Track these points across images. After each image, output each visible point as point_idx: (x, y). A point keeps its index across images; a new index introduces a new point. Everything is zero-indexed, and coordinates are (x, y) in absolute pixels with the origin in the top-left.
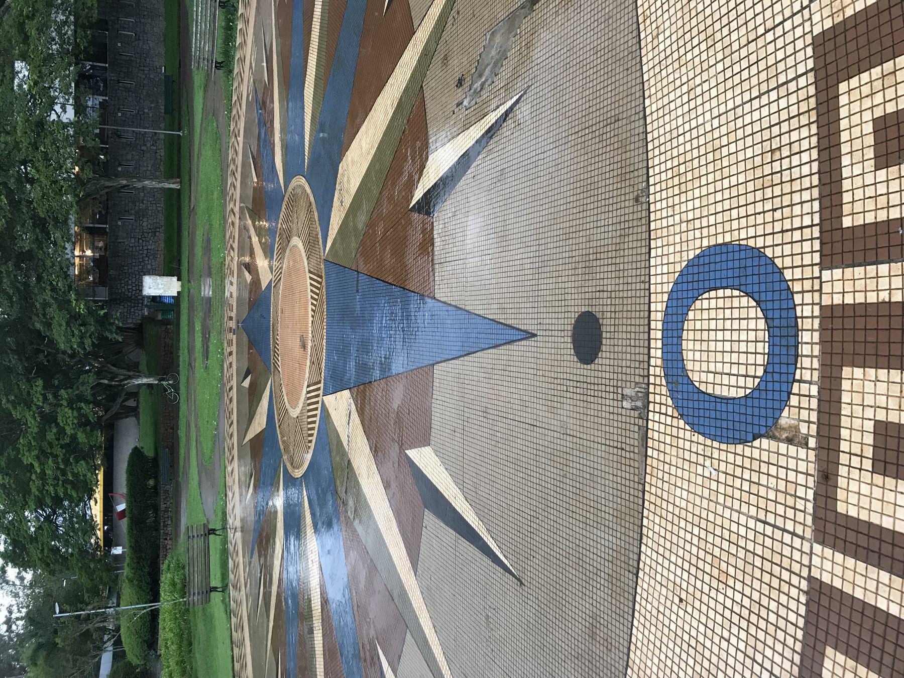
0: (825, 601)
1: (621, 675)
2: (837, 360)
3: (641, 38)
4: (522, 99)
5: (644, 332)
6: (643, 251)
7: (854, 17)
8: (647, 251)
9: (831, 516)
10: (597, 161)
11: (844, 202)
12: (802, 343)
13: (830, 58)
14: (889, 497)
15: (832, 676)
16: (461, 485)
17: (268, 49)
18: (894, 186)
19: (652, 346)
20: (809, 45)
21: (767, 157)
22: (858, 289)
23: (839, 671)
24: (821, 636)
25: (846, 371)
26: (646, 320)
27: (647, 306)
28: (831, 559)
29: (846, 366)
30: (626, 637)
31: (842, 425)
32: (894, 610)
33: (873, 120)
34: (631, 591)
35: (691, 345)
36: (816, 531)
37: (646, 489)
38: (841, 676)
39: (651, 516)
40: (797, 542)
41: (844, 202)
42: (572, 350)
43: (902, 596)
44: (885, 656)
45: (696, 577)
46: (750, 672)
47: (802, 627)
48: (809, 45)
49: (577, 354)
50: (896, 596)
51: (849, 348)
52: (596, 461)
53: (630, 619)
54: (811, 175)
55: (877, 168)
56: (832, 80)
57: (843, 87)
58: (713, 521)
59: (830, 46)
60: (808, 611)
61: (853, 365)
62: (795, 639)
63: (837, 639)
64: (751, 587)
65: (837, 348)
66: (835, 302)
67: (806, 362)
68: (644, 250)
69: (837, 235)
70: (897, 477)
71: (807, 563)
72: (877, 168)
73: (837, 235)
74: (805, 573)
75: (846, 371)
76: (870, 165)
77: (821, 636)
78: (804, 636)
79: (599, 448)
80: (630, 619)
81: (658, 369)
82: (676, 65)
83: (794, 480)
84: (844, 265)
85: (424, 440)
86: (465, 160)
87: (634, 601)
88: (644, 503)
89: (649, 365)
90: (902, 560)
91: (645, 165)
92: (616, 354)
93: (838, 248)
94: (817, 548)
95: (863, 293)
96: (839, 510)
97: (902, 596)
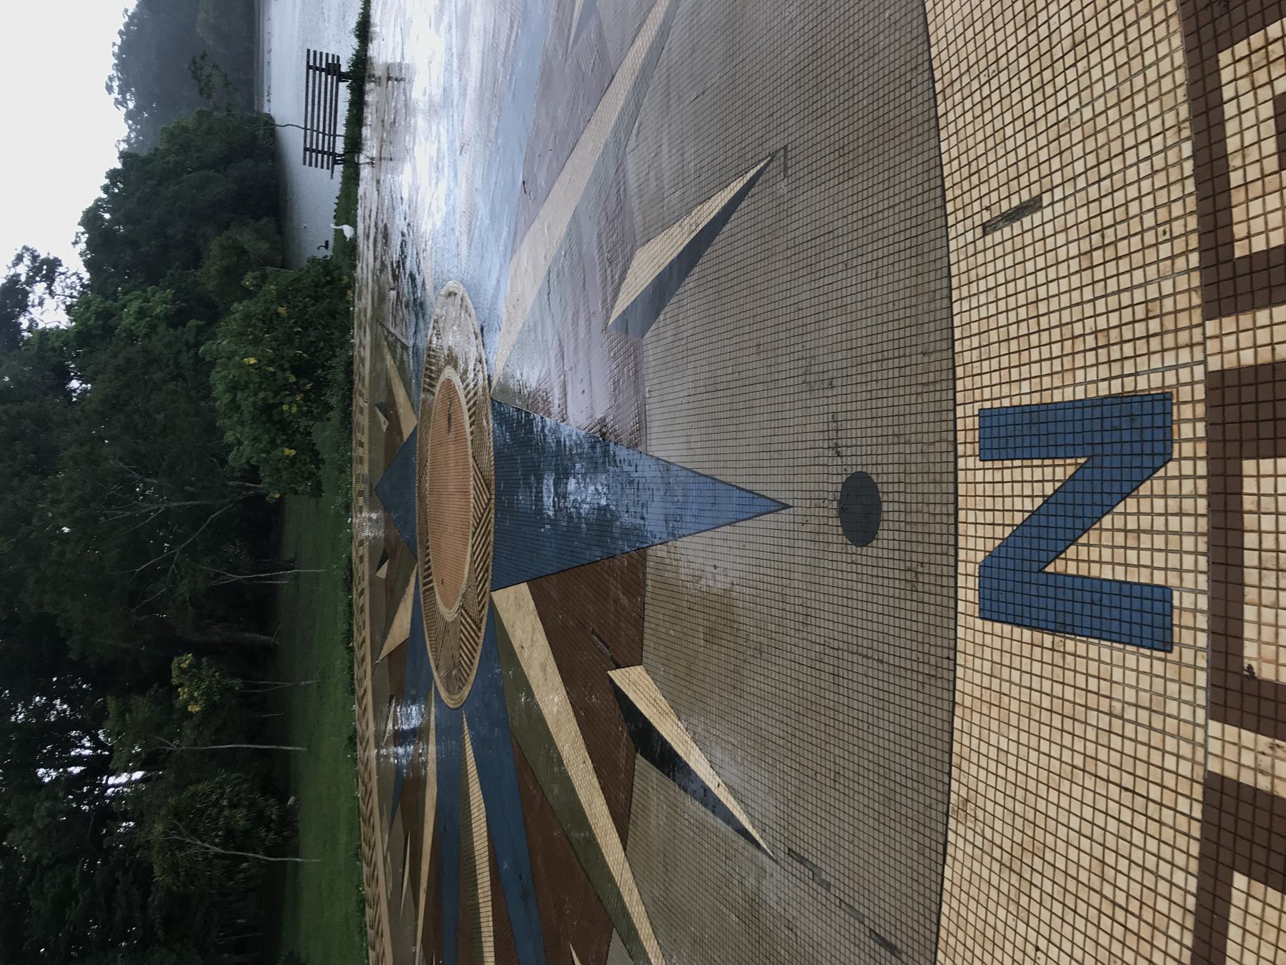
0: (1229, 804)
2: (1232, 450)
3: (930, 33)
5: (948, 576)
6: (944, 347)
8: (950, 356)
9: (1233, 682)
10: (870, 203)
12: (1179, 403)
19: (960, 493)
24: (1225, 856)
25: (1249, 466)
26: (951, 392)
27: (951, 424)
29: (1248, 458)
34: (934, 898)
37: (954, 750)
39: (965, 765)
42: (840, 529)
49: (847, 533)
53: (934, 929)
57: (1225, 57)
60: (1199, 905)
61: (1258, 456)
62: (1183, 927)
65: (1232, 432)
67: (1186, 430)
68: (945, 345)
73: (1226, 271)
75: (1249, 466)
77: (1225, 856)
80: (934, 929)
81: (971, 579)
82: (978, 110)
83: (1174, 769)
84: (1236, 311)
85: (633, 658)
87: (939, 913)
89: (956, 613)
91: (938, 172)
94: (1215, 727)
95: (1262, 473)
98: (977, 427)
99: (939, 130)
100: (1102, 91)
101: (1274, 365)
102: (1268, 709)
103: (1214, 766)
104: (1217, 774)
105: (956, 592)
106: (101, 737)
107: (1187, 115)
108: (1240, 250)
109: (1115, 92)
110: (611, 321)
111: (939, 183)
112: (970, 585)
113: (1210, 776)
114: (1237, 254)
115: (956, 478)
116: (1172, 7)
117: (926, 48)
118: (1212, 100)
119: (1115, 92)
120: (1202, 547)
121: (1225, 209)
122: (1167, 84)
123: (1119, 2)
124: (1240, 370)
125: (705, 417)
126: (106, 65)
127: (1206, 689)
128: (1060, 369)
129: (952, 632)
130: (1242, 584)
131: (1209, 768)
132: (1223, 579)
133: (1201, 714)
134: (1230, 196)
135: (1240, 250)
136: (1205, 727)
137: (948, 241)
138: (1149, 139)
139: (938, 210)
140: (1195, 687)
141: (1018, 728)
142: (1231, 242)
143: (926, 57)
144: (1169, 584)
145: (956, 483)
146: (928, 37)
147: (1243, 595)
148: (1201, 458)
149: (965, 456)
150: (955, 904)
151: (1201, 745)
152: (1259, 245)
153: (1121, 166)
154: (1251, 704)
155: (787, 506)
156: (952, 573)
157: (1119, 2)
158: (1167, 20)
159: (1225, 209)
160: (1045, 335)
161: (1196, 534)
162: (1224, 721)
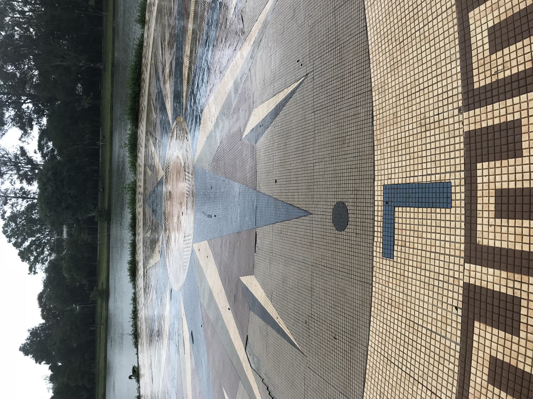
11: (483, 267)
14: (525, 287)
16: (270, 296)
18: (527, 49)
20: (455, 18)
21: (444, 76)
25: (479, 165)
26: (373, 156)
28: (486, 347)
32: (528, 369)
33: (521, 298)
41: (483, 267)
43: (532, 369)
44: (520, 383)
45: (414, 316)
46: (444, 371)
48: (455, 18)
50: (529, 361)
52: (348, 272)
54: (460, 143)
55: (520, 120)
56: (465, 12)
58: (413, 320)
64: (440, 349)
68: (371, 213)
70: (528, 275)
72: (520, 120)
76: (515, 339)
79: (346, 270)
90: (532, 349)
92: (365, 192)
97: (532, 369)
98: (382, 205)
100: (430, 59)
105: (374, 172)
106: (14, 225)
107: (459, 57)
108: (476, 86)
110: (246, 133)
111: (371, 109)
112: (379, 235)
114: (475, 87)
115: (374, 148)
120: (463, 205)
122: (451, 31)
125: (278, 242)
126: (37, 297)
127: (462, 309)
129: (371, 273)
133: (462, 261)
135: (476, 86)
136: (464, 266)
138: (445, 52)
139: (371, 208)
140: (459, 294)
142: (473, 83)
143: (369, 77)
145: (374, 170)
151: (462, 272)
152: (482, 83)
155: (311, 214)
156: (371, 271)
157: (434, 1)
158: (453, 26)
160: (408, 152)
161: (460, 257)
162: (470, 263)
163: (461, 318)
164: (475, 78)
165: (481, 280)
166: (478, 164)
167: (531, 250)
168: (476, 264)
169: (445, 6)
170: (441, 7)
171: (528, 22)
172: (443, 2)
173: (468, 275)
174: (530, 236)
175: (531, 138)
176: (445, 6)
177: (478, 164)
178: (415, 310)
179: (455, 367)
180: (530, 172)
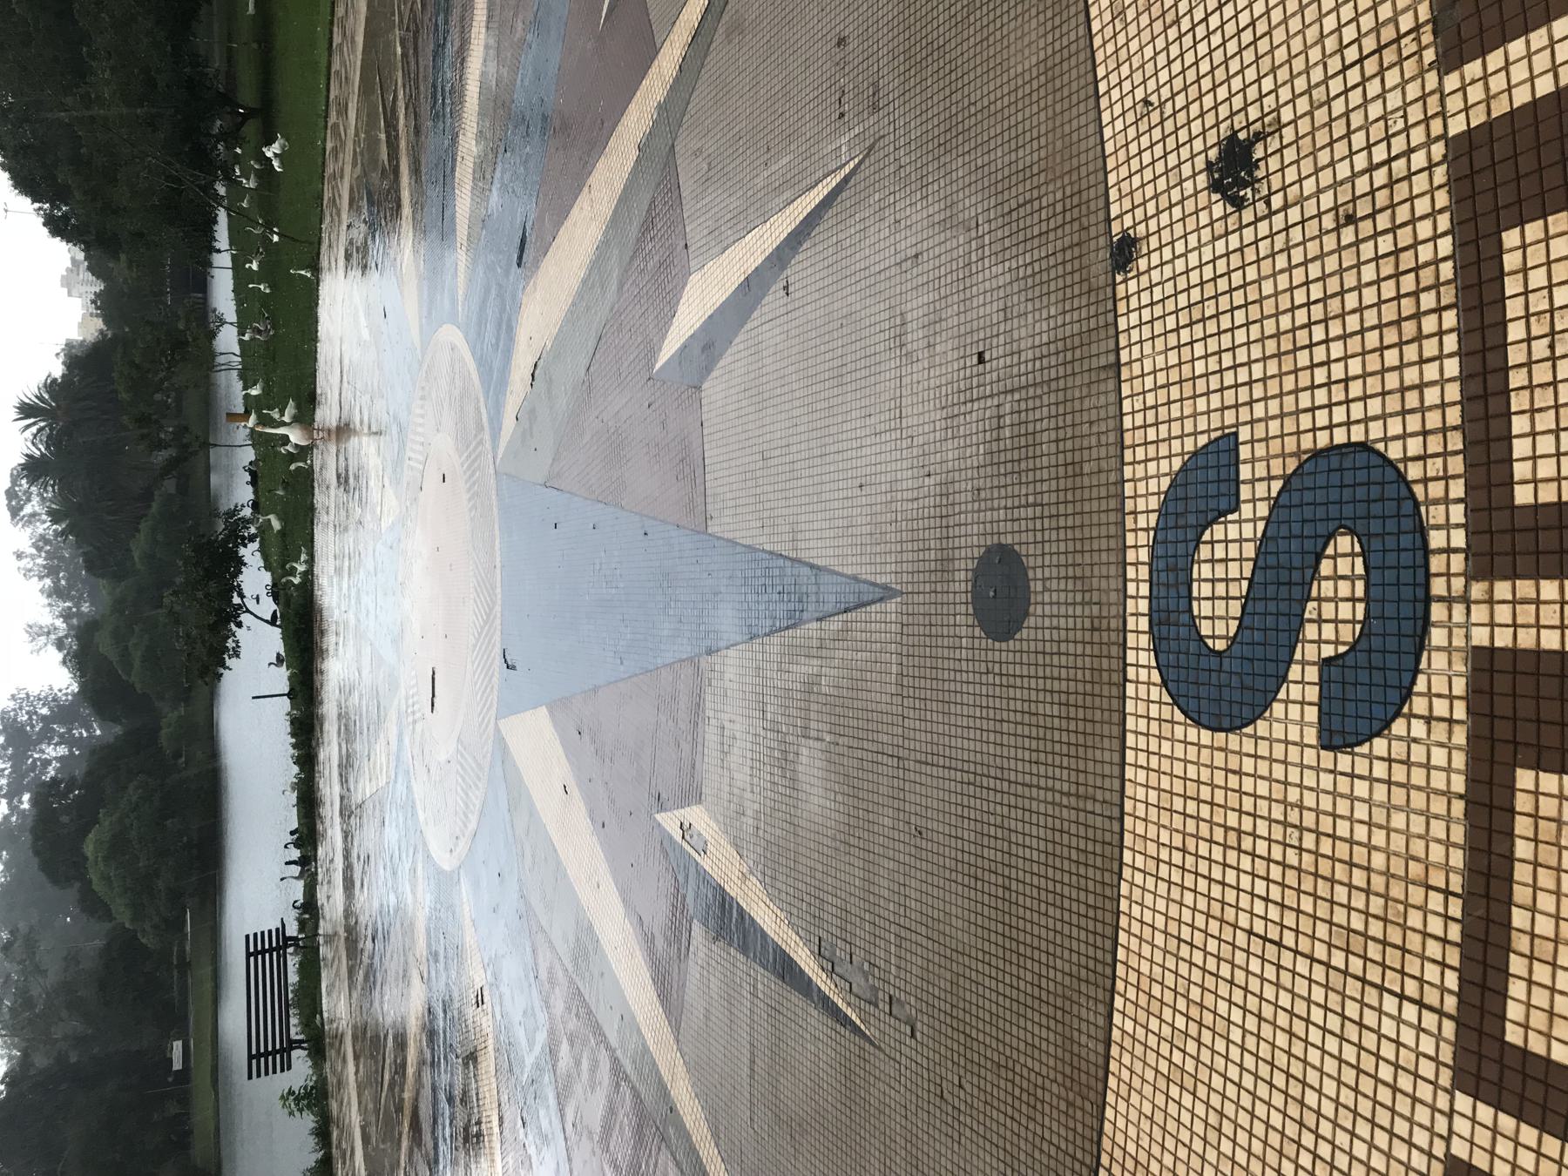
1: (1085, 1172)
4: (852, 182)
7: (1466, 985)
9: (1491, 1049)
13: (1483, 182)
15: (1513, 1172)
17: (389, 105)
22: (1557, 543)
23: (1527, 1160)
30: (1101, 1008)
31: (1518, 809)
35: (1206, 590)
36: (1457, 1070)
38: (1532, 1169)
40: (1430, 1020)
47: (1459, 891)
51: (1526, 732)
56: (1485, 225)
59: (1481, 158)
63: (1522, 1097)
66: (1498, 643)
69: (1500, 520)
71: (1446, 1108)
74: (1439, 1149)
78: (1524, 107)
86: (751, 289)
88: (1114, 984)
93: (1503, 543)
94: (1463, 1102)
96: (1509, 1038)
99: (1106, 174)
101: (1560, 94)
102: (1535, 1091)
103: (1459, 1149)
104: (1462, 1161)
109: (1355, 46)
113: (1470, 576)
116: (1424, 12)
117: (1089, 67)
118: (1476, 387)
119: (1355, 46)
121: (1495, 302)
123: (1352, 4)
124: (1513, 575)
128: (1264, 474)
130: (1512, 812)
131: (1454, 1151)
132: (1492, 436)
134: (1489, 1104)
135: (1524, 778)
137: (1116, 317)
141: (1208, 896)
144: (1414, 698)
146: (1093, 53)
147: (1514, 780)
148: (1458, 526)
149: (1135, 598)
150: (1125, 1075)
153: (1353, 239)
154: (1513, 1081)
157: (1352, 4)
159: (1495, 302)
163: (1456, 974)
164: (1511, 327)
165: (1515, 743)
166: (1504, 235)
167: (1564, 499)
168: (1505, 345)
169: (1267, 59)
170: (1236, 16)
171: (1518, 178)
172: (1259, 8)
173: (1487, 711)
174: (1558, 455)
175: (1562, 401)
176: (1267, 59)
177: (1504, 235)
178: (1205, 932)
179: (1440, 1092)
180: (1557, 407)
